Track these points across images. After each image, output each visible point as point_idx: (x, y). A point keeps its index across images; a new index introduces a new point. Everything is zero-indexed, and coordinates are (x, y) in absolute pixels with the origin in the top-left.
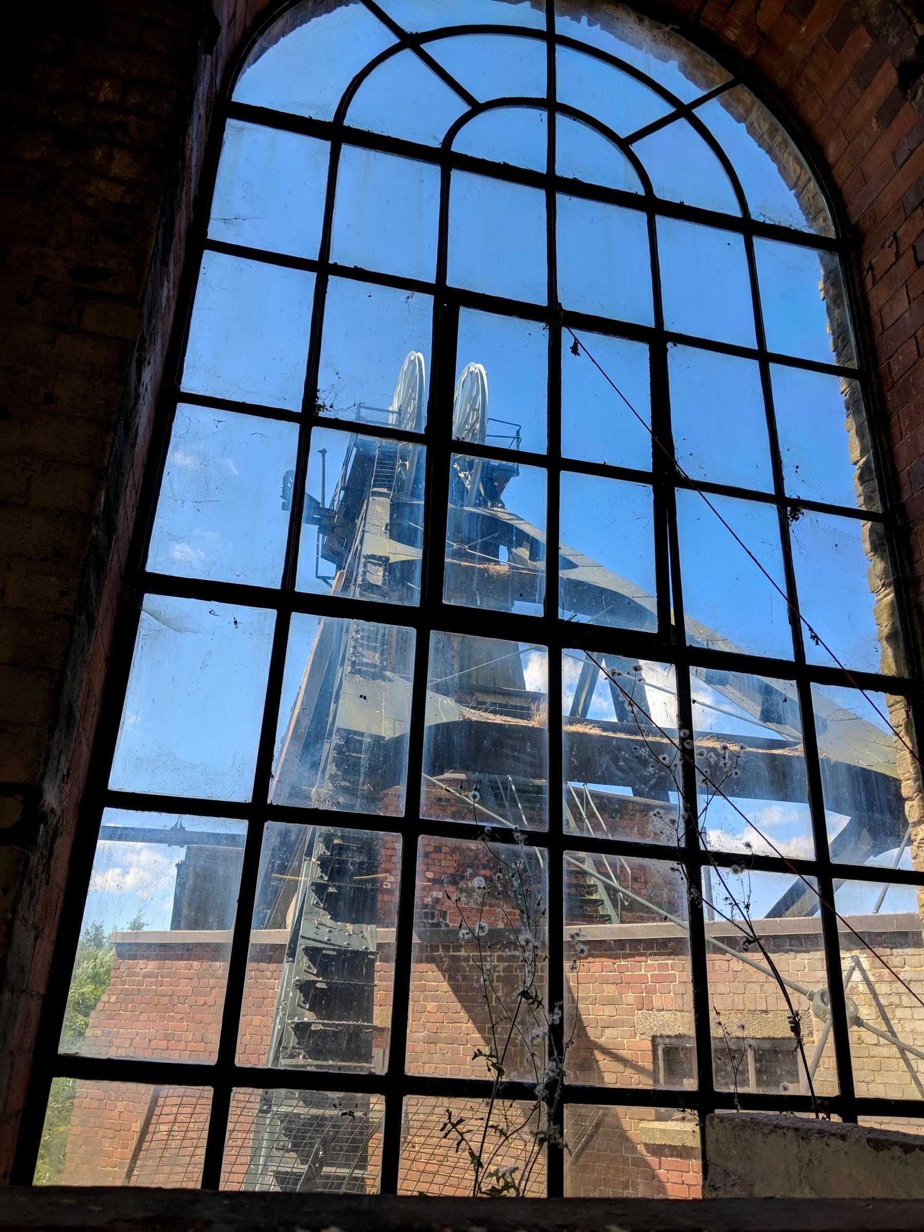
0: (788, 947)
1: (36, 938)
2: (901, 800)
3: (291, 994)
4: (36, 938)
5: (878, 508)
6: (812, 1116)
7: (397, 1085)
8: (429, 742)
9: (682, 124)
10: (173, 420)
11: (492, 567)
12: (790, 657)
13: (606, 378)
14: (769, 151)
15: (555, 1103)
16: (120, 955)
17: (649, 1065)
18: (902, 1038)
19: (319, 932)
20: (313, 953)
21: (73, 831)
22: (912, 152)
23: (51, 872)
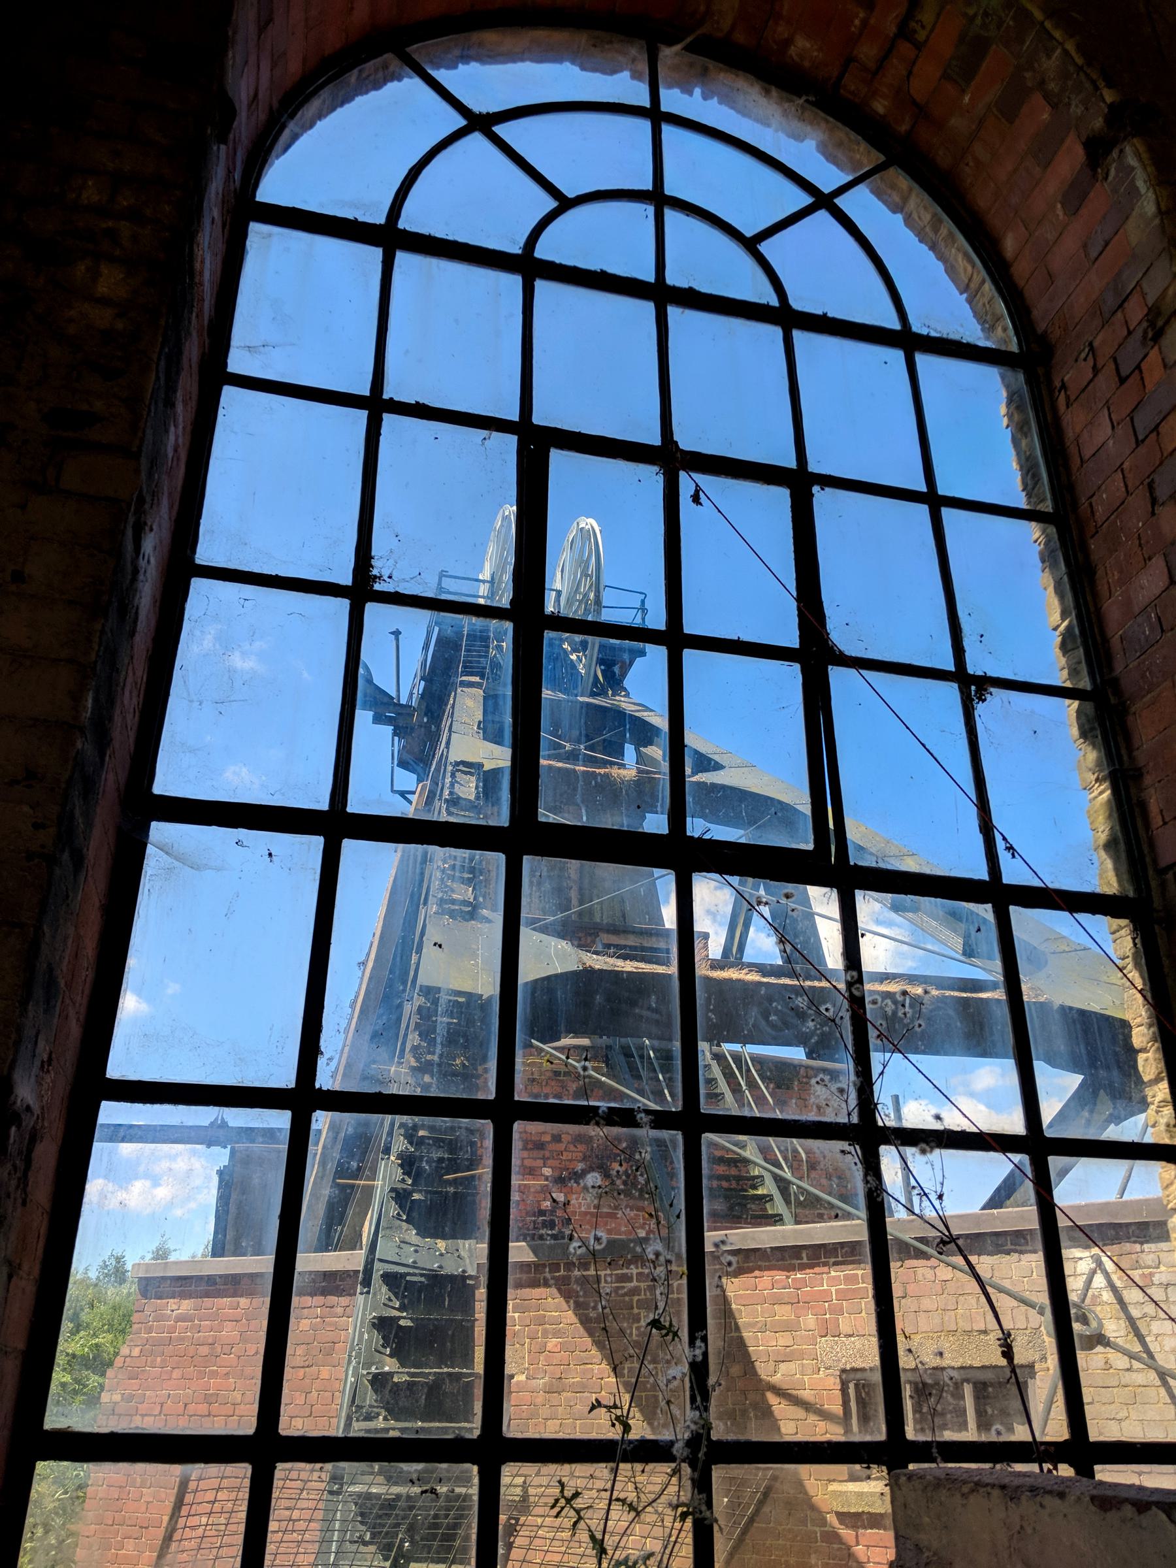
0: (1009, 1247)
2: (1132, 1052)
3: (366, 1336)
4: (10, 1277)
5: (1085, 683)
6: (1034, 1468)
7: (494, 1450)
8: (524, 998)
9: (822, 215)
10: (186, 600)
11: (615, 771)
12: (982, 874)
13: (737, 533)
14: (933, 247)
15: (700, 1465)
16: (144, 1293)
17: (837, 1408)
18: (1161, 1359)
19: (401, 1252)
20: (390, 1279)
21: (60, 1134)
22: (1107, 244)
23: (29, 1189)
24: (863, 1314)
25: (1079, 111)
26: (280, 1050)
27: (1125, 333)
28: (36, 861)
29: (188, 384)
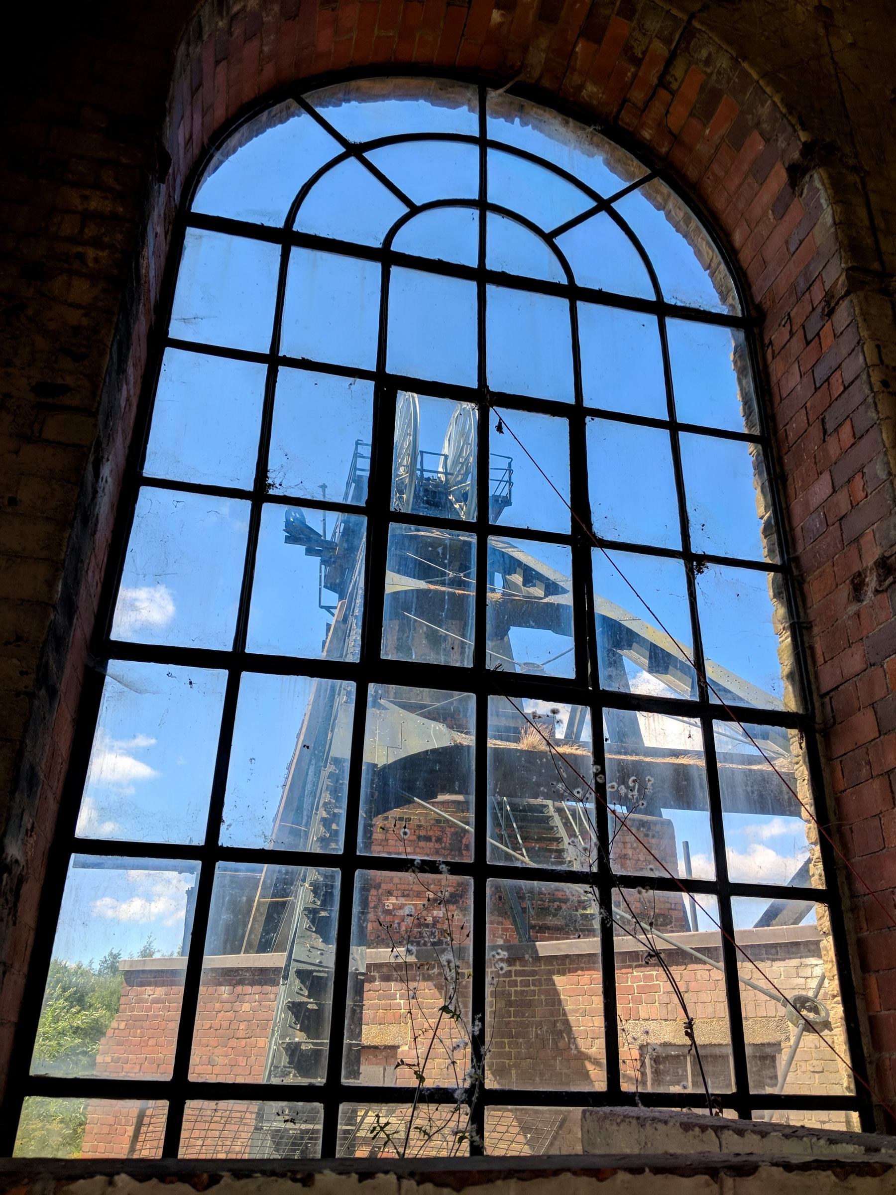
1: (4, 973)
4: (4, 973)
6: (706, 1111)
9: (603, 215)
13: (530, 453)
19: (310, 955)
21: (42, 876)
23: (19, 914)
24: (657, 1004)
25: (783, 146)
26: (194, 819)
27: (811, 308)
28: (22, 696)
29: (139, 350)
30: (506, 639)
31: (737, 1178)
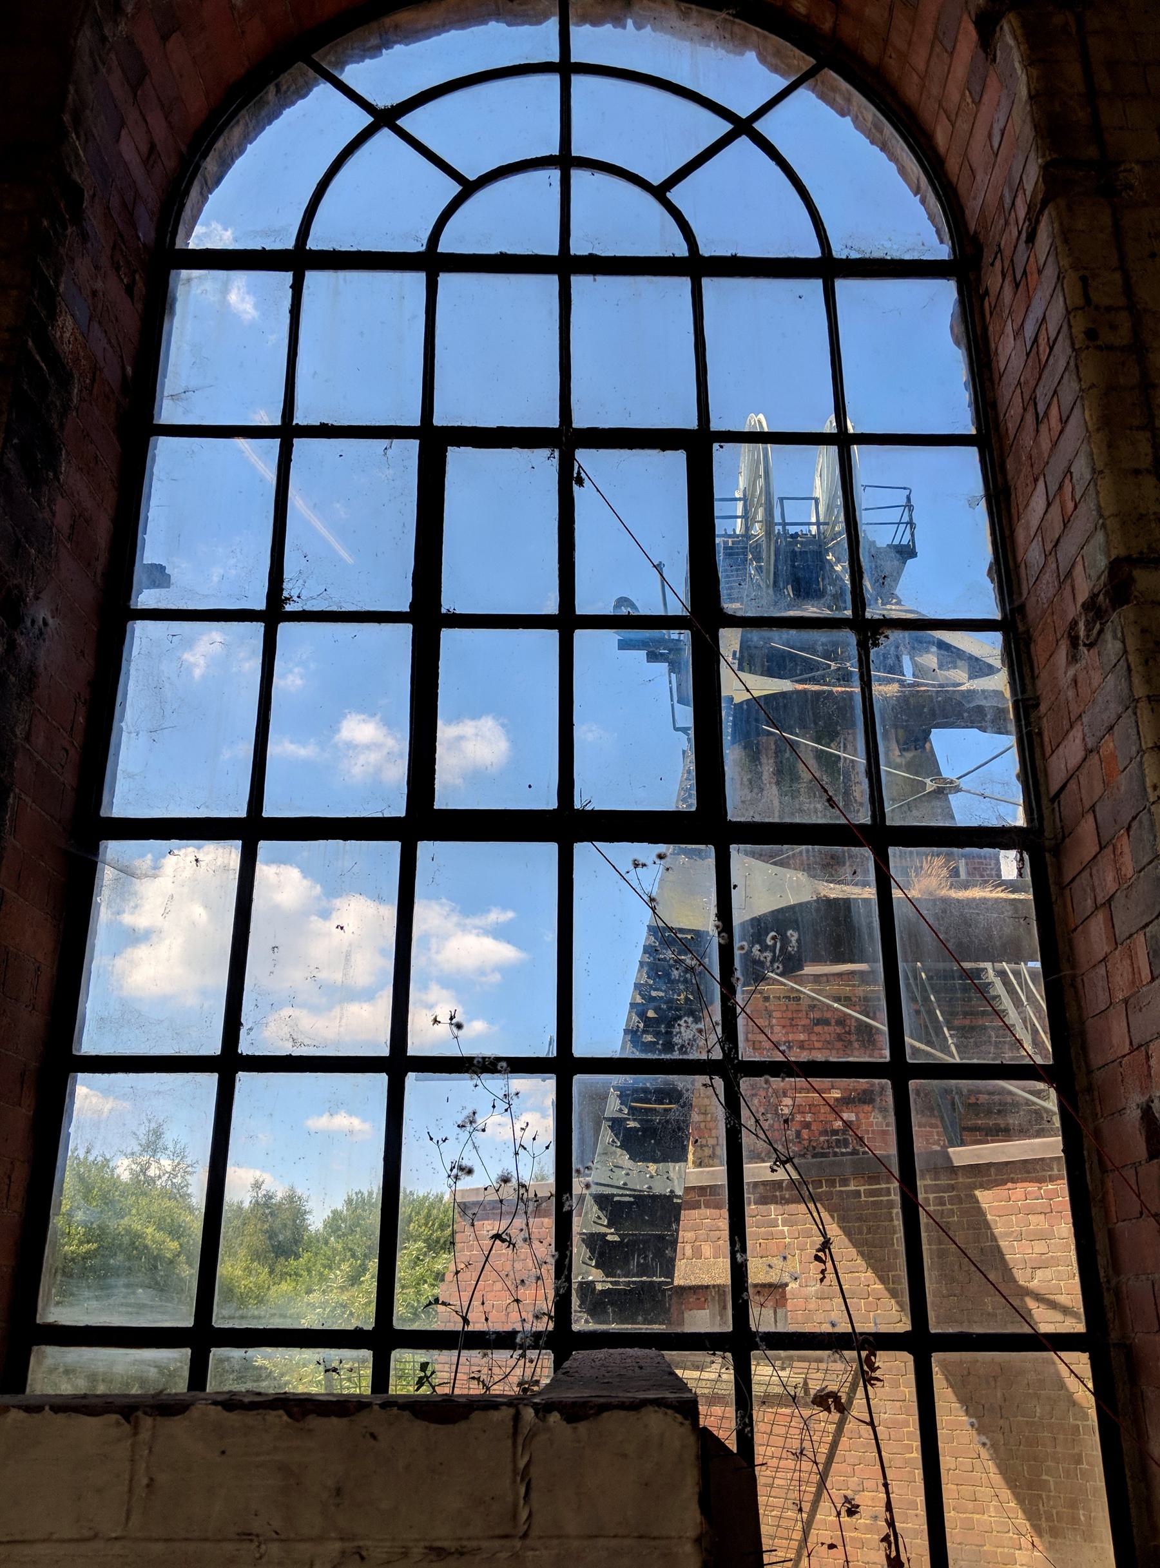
30: (927, 745)
31: (158, 1418)
